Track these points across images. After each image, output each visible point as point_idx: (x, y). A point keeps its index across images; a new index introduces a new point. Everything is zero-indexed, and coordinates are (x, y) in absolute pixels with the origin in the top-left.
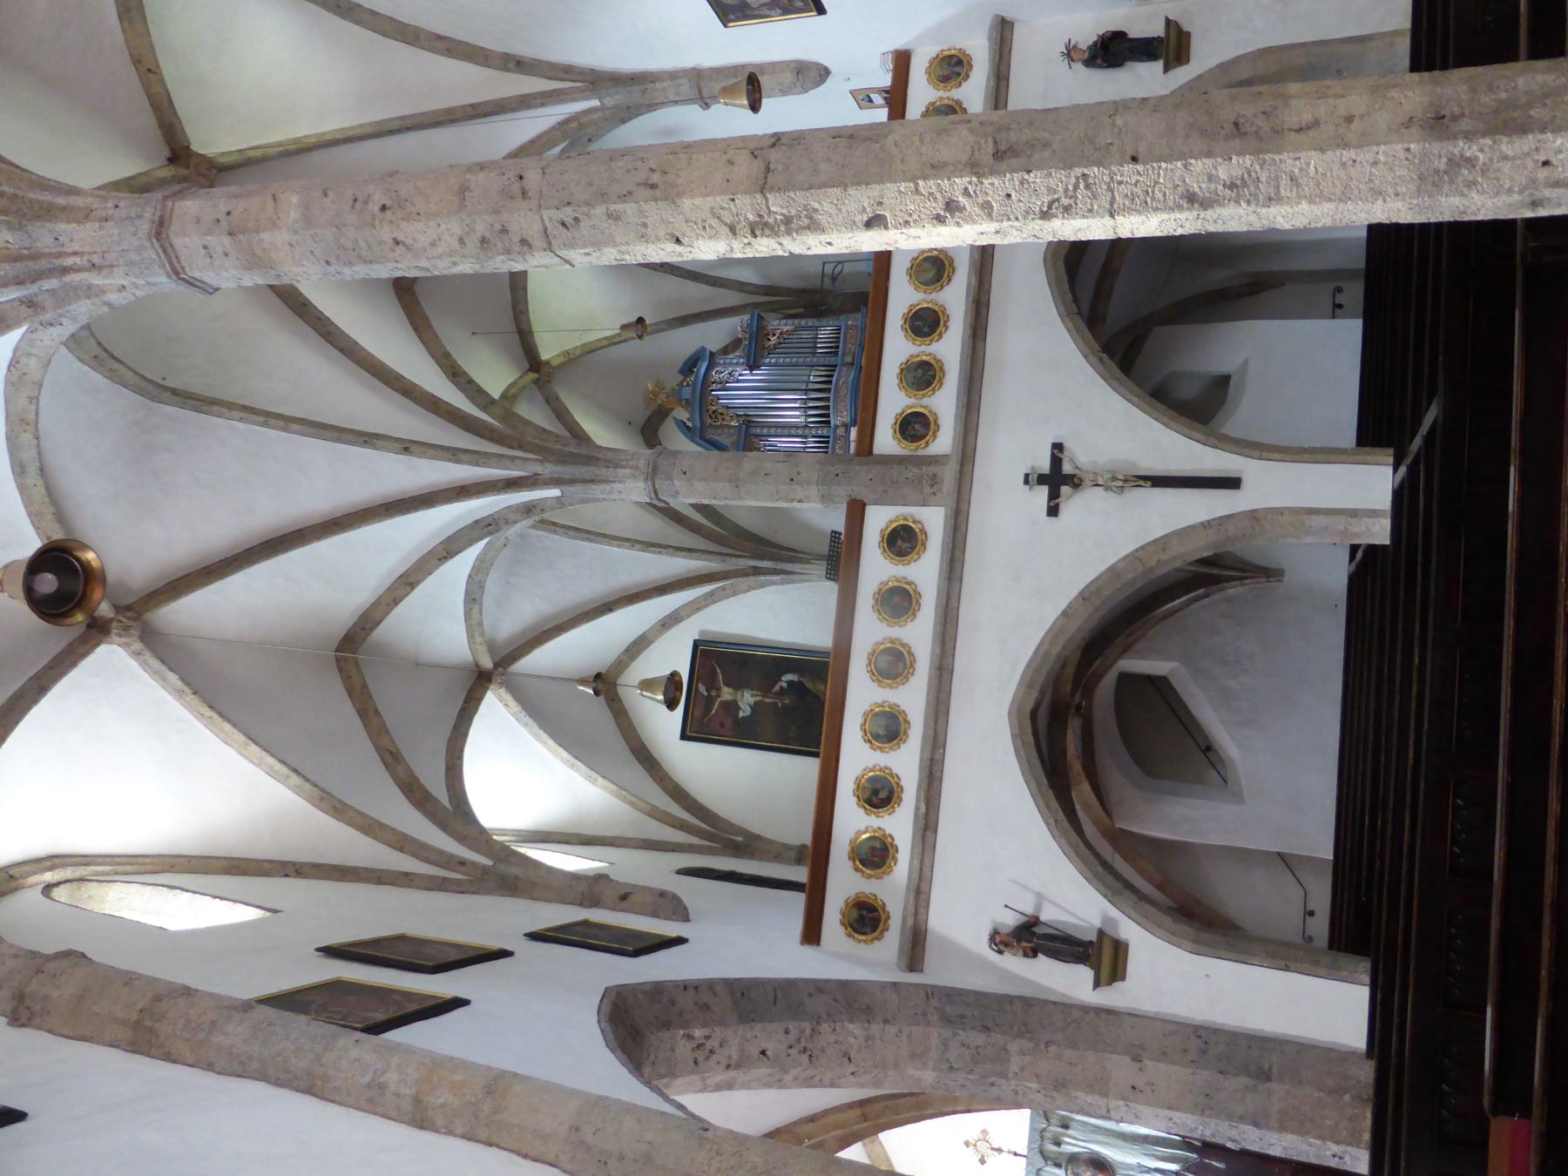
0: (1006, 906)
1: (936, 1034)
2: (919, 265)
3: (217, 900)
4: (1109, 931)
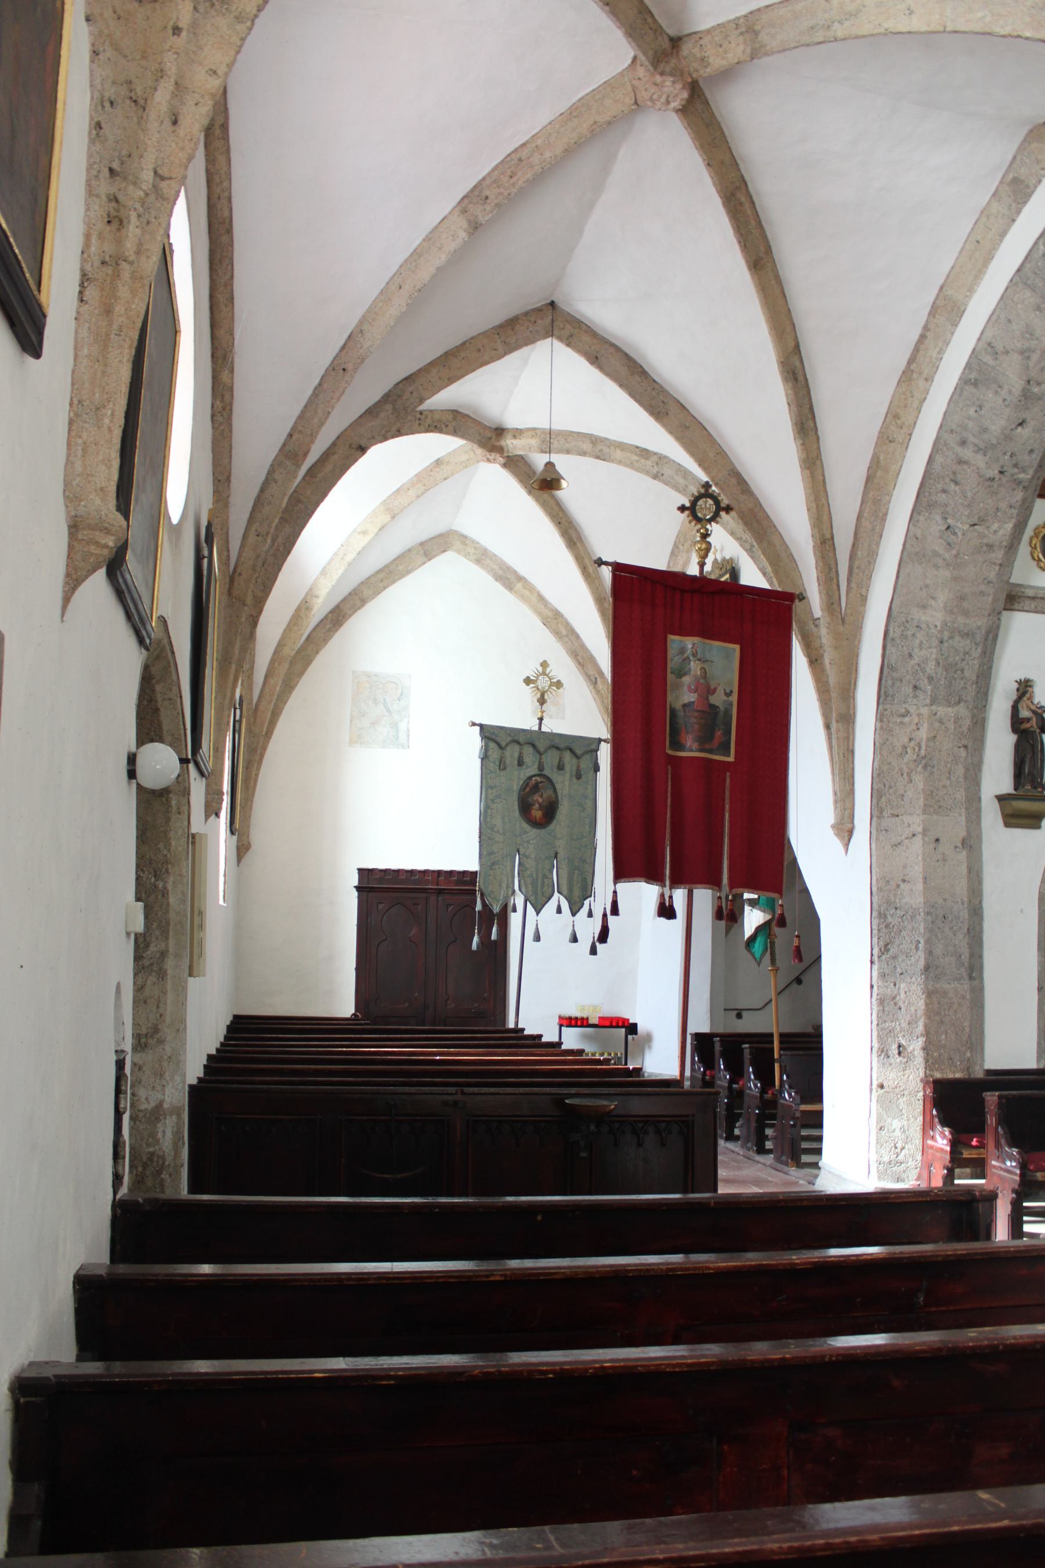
1: (979, 623)
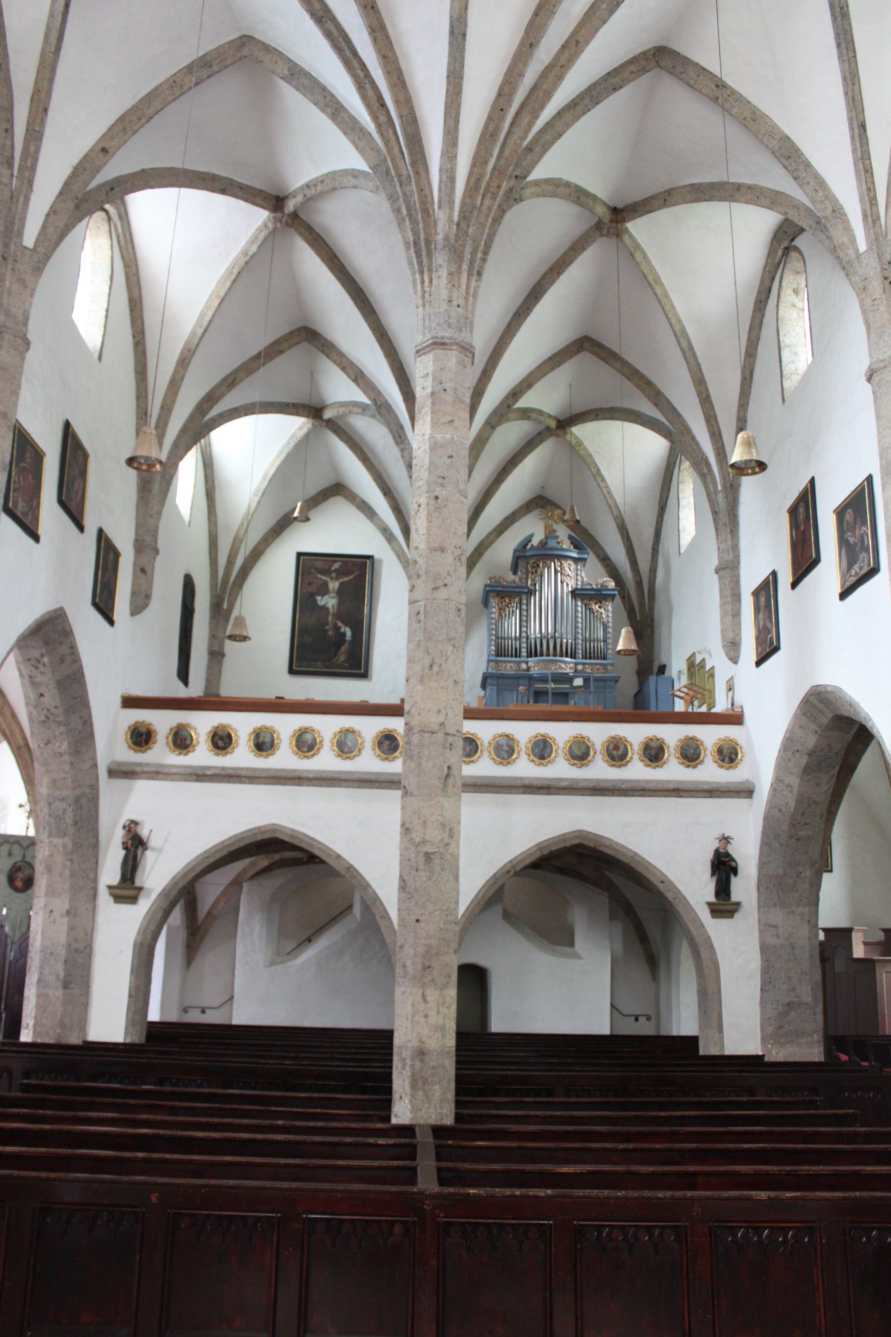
0: (151, 831)
2: (584, 743)
3: (105, 313)
4: (142, 893)
